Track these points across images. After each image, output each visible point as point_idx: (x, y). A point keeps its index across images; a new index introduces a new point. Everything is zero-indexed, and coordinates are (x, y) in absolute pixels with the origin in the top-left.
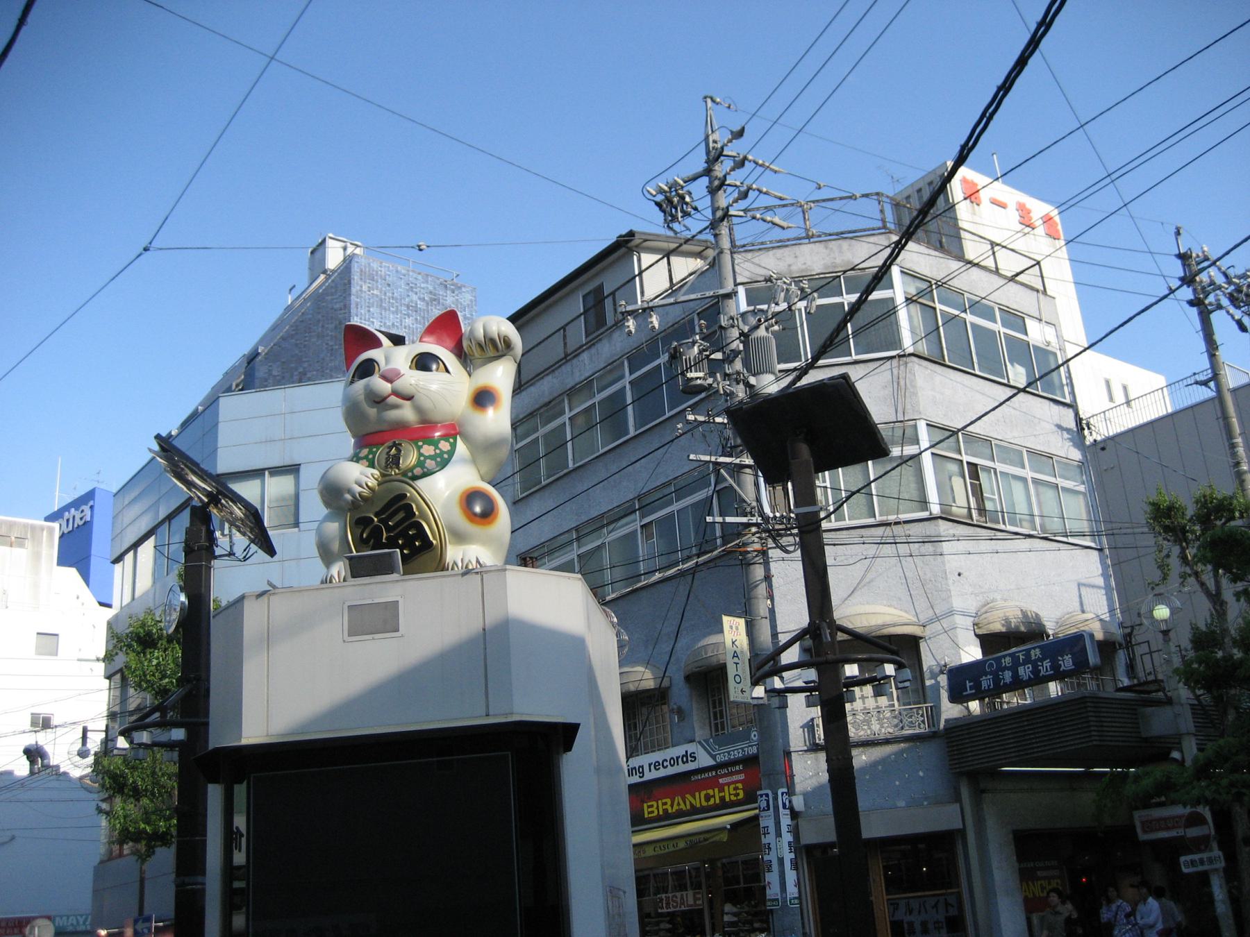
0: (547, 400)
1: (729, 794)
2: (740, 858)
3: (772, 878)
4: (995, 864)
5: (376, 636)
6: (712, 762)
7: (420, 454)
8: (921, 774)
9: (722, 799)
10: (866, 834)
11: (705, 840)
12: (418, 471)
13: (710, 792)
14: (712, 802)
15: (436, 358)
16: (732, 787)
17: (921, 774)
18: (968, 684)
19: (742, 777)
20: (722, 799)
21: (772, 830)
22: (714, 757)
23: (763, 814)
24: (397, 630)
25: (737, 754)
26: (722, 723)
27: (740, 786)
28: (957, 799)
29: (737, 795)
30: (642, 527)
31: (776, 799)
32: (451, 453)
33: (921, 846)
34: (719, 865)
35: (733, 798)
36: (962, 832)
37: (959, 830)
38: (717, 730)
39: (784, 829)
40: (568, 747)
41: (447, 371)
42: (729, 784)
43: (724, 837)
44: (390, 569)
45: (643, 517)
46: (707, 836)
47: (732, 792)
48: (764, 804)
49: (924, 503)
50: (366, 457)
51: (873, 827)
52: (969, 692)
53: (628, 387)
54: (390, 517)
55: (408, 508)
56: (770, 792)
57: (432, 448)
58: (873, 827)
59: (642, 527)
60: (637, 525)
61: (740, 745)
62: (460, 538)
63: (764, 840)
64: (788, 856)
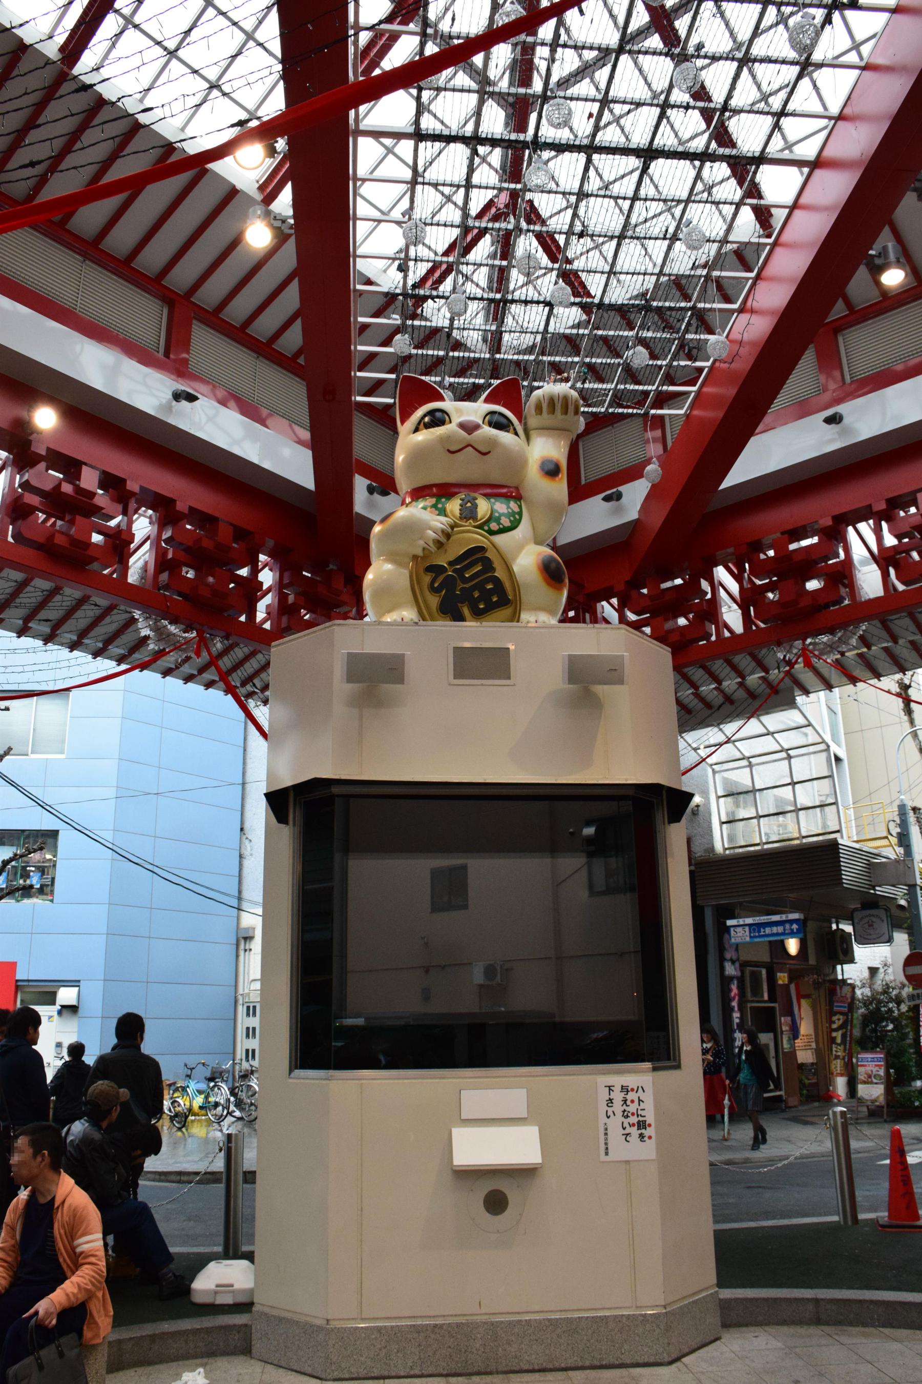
12: (494, 526)
55: (488, 565)
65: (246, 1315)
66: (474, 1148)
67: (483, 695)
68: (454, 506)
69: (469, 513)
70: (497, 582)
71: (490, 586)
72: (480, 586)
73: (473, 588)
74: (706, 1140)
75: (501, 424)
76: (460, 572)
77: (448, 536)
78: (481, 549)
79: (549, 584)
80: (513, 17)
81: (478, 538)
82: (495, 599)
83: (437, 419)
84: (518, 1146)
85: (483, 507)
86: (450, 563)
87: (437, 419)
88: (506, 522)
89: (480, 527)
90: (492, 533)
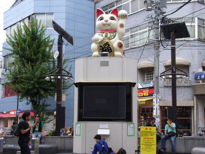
0: (111, 3)
1: (145, 94)
2: (146, 107)
3: (155, 111)
4: (200, 114)
5: (105, 66)
6: (142, 87)
7: (110, 35)
8: (186, 94)
9: (143, 95)
10: (177, 105)
11: (140, 103)
12: (110, 38)
13: (141, 93)
14: (141, 95)
15: (114, 18)
16: (146, 93)
17: (186, 94)
18: (199, 77)
19: (148, 91)
20: (143, 95)
21: (155, 102)
22: (142, 86)
23: (154, 99)
24: (108, 66)
25: (148, 86)
26: (145, 79)
27: (147, 93)
28: (193, 100)
29: (146, 94)
30: (131, 35)
31: (157, 96)
32: (116, 35)
33: (184, 109)
34: (141, 108)
35: (146, 95)
36: (193, 107)
37: (193, 106)
38: (143, 81)
39: (158, 102)
40: (134, 86)
41: (115, 20)
42: (145, 92)
43: (144, 103)
44: (107, 56)
45: (131, 33)
46: (141, 102)
47: (146, 94)
48: (154, 97)
49: (194, 37)
50: (101, 35)
51: (178, 104)
52: (199, 78)
53: (130, 2)
54: (106, 46)
55: (109, 45)
56: (156, 95)
57: (113, 34)
58: (178, 104)
59: (131, 35)
60: (130, 35)
61: (148, 84)
62: (117, 51)
63: (154, 104)
64: (158, 108)
65: (56, 100)
66: (100, 132)
67: (104, 68)
68: (104, 35)
69: (106, 36)
70: (110, 48)
71: (109, 49)
72: (108, 49)
73: (107, 49)
74: (2, 48)
75: (112, 18)
76: (105, 46)
77: (103, 40)
78: (108, 43)
79: (120, 48)
80: (63, 55)
81: (107, 41)
82: (110, 51)
83: (102, 19)
84: (106, 132)
85: (109, 35)
86: (103, 45)
87: (102, 19)
88: (112, 37)
89: (108, 39)
90: (110, 39)
